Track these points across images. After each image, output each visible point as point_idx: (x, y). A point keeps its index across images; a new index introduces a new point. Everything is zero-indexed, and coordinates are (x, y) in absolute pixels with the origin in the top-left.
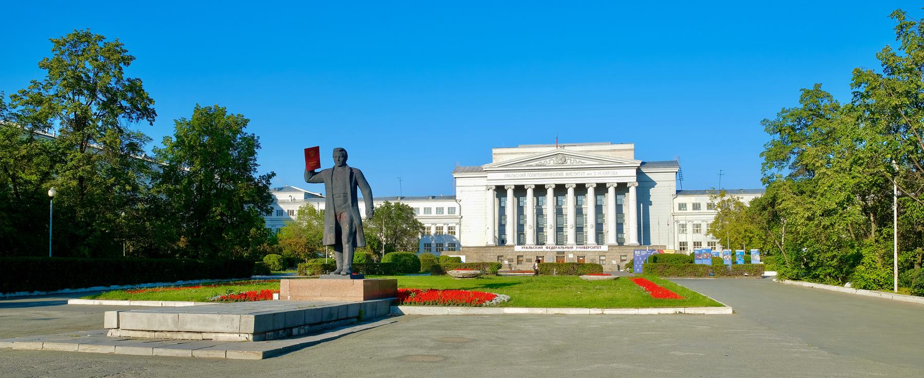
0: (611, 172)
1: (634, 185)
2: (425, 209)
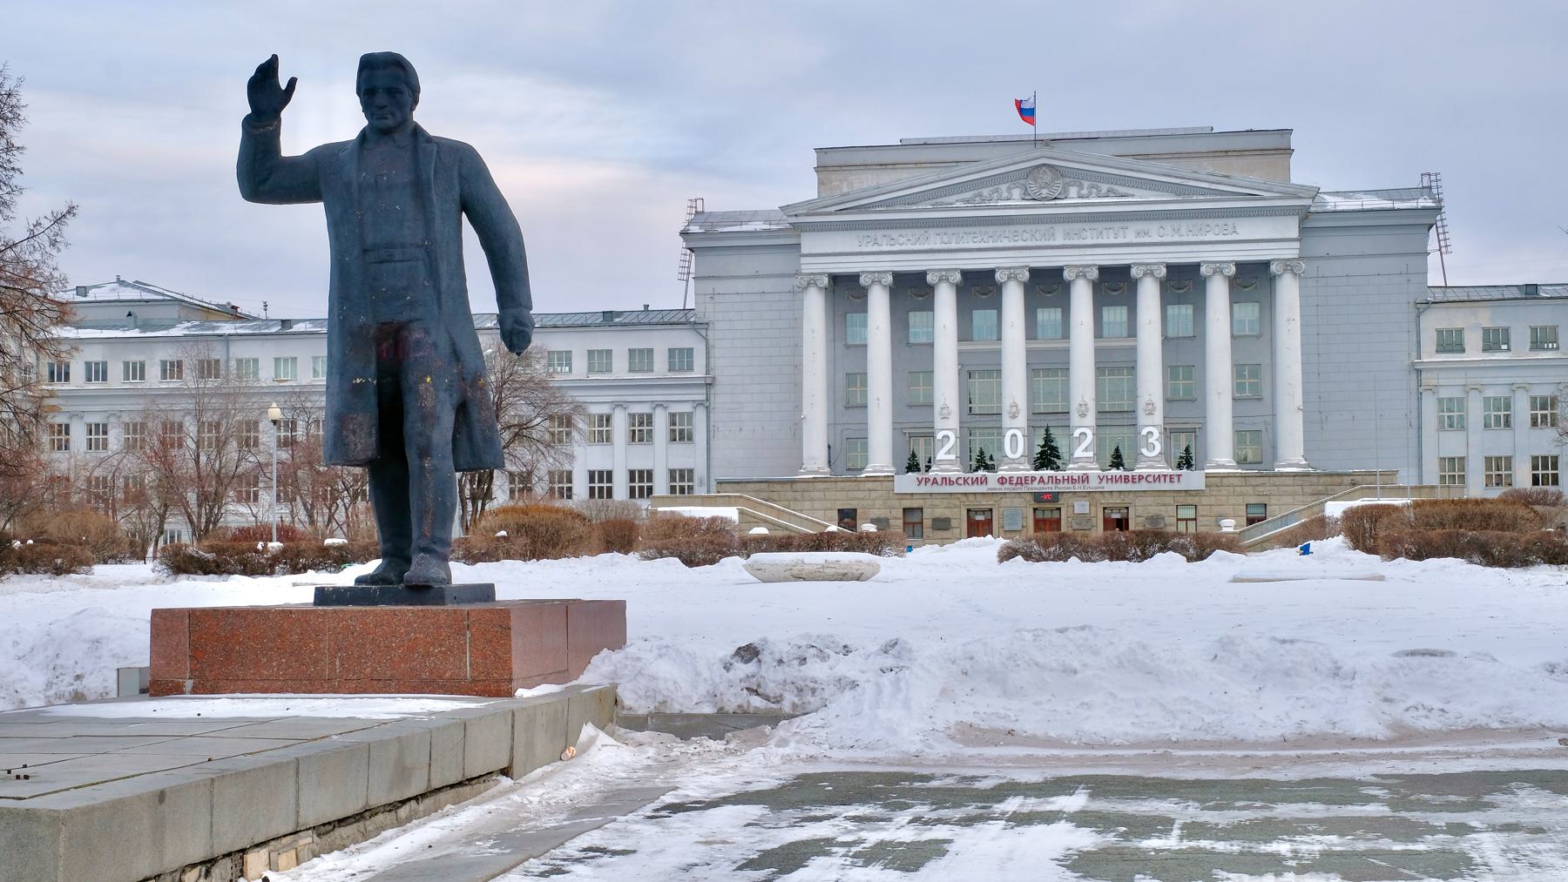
0: (1213, 230)
1: (1152, 274)
2: (671, 351)
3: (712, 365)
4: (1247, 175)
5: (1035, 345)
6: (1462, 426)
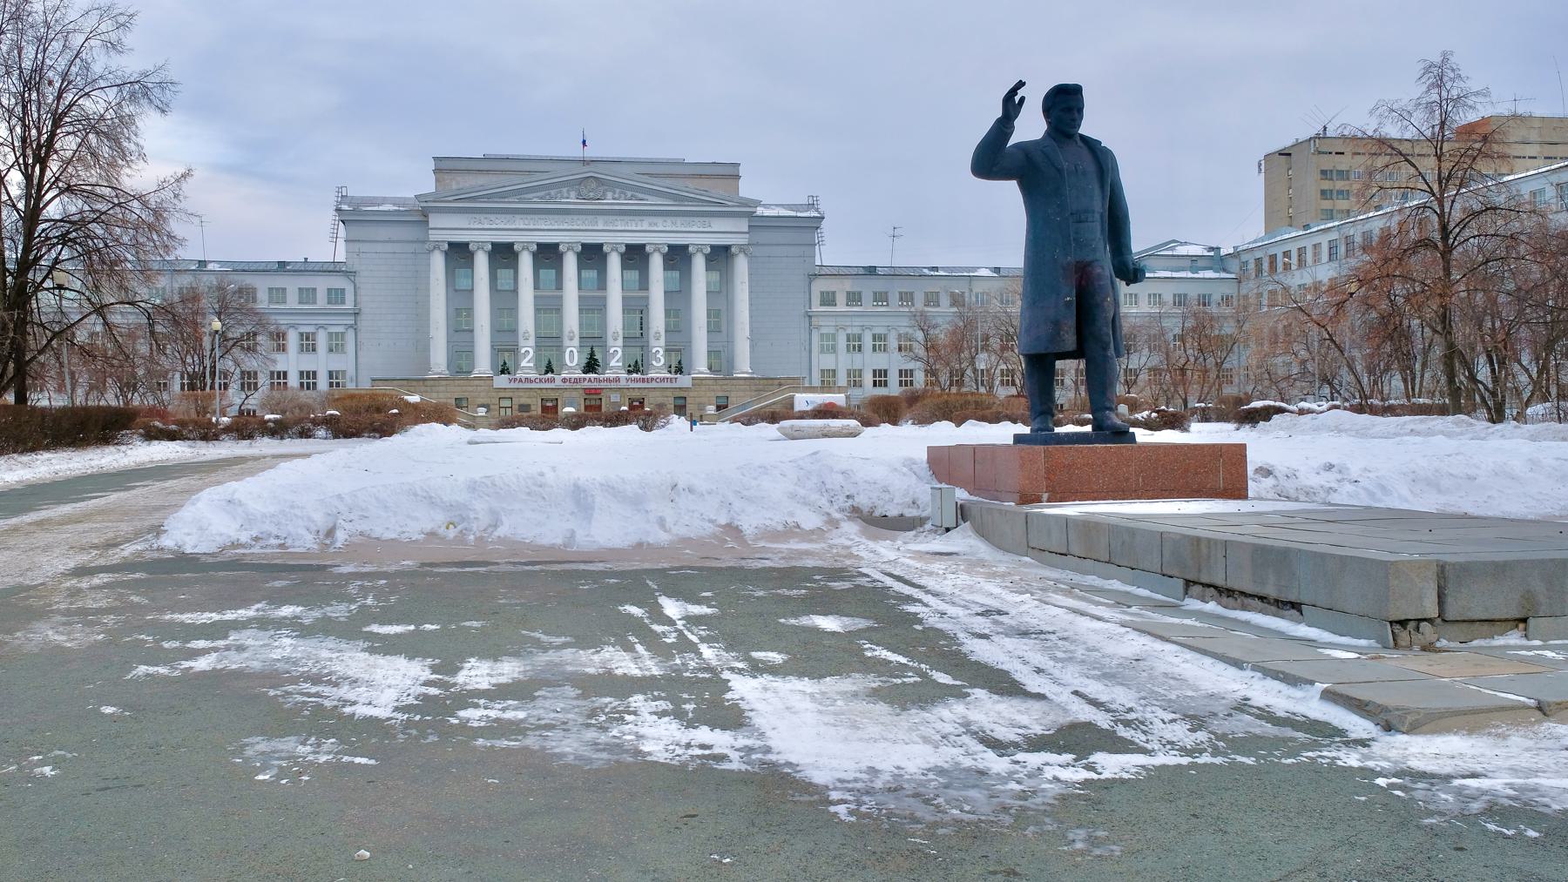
1: (659, 250)
3: (358, 300)
4: (718, 190)
5: (539, 293)
6: (834, 349)
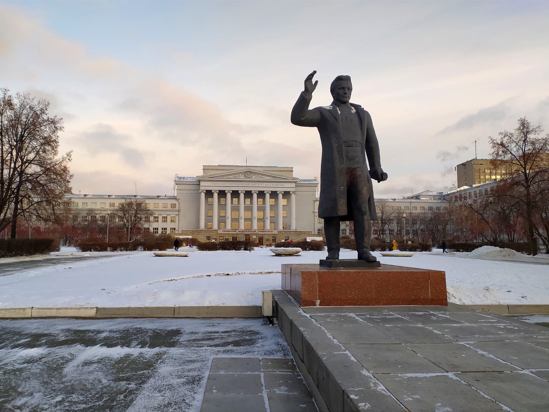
0: (280, 185)
1: (268, 193)
